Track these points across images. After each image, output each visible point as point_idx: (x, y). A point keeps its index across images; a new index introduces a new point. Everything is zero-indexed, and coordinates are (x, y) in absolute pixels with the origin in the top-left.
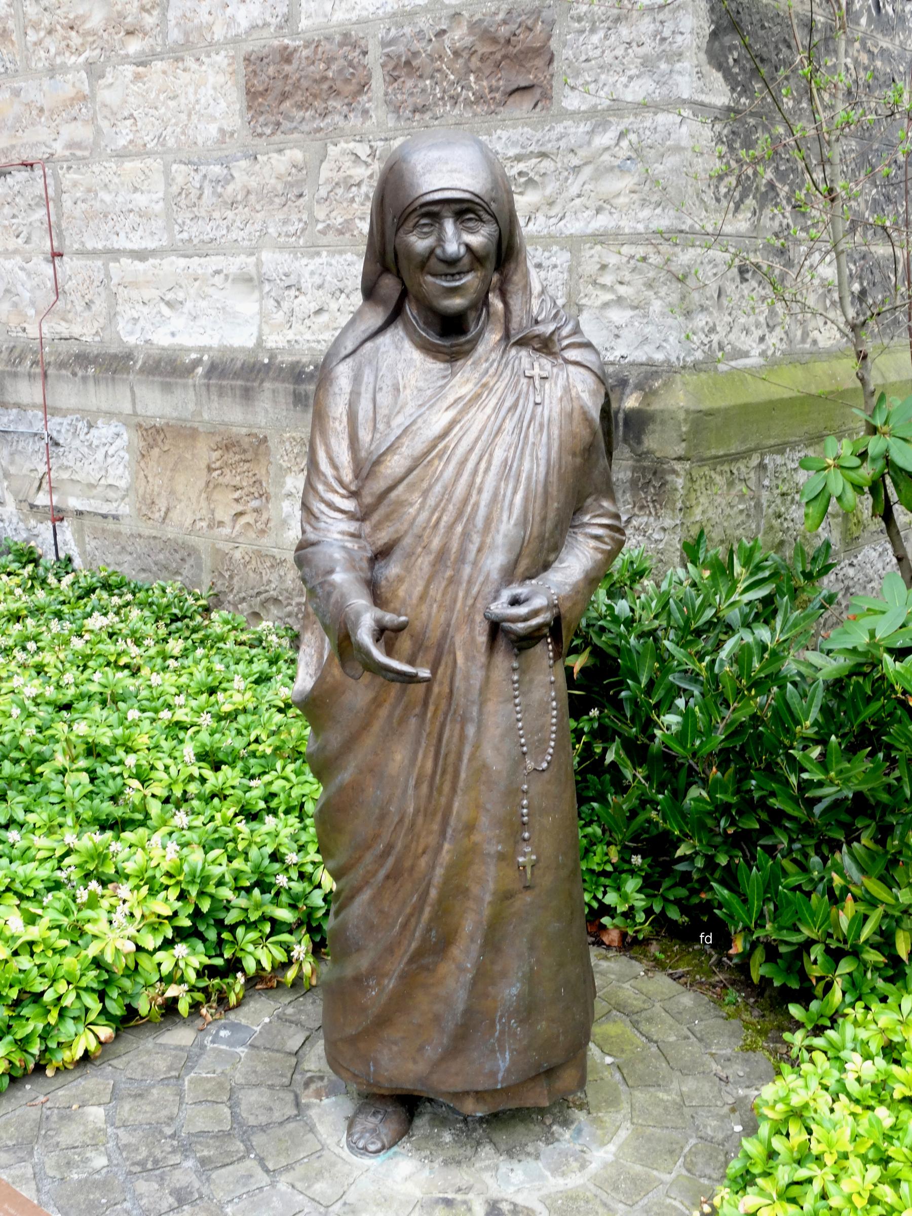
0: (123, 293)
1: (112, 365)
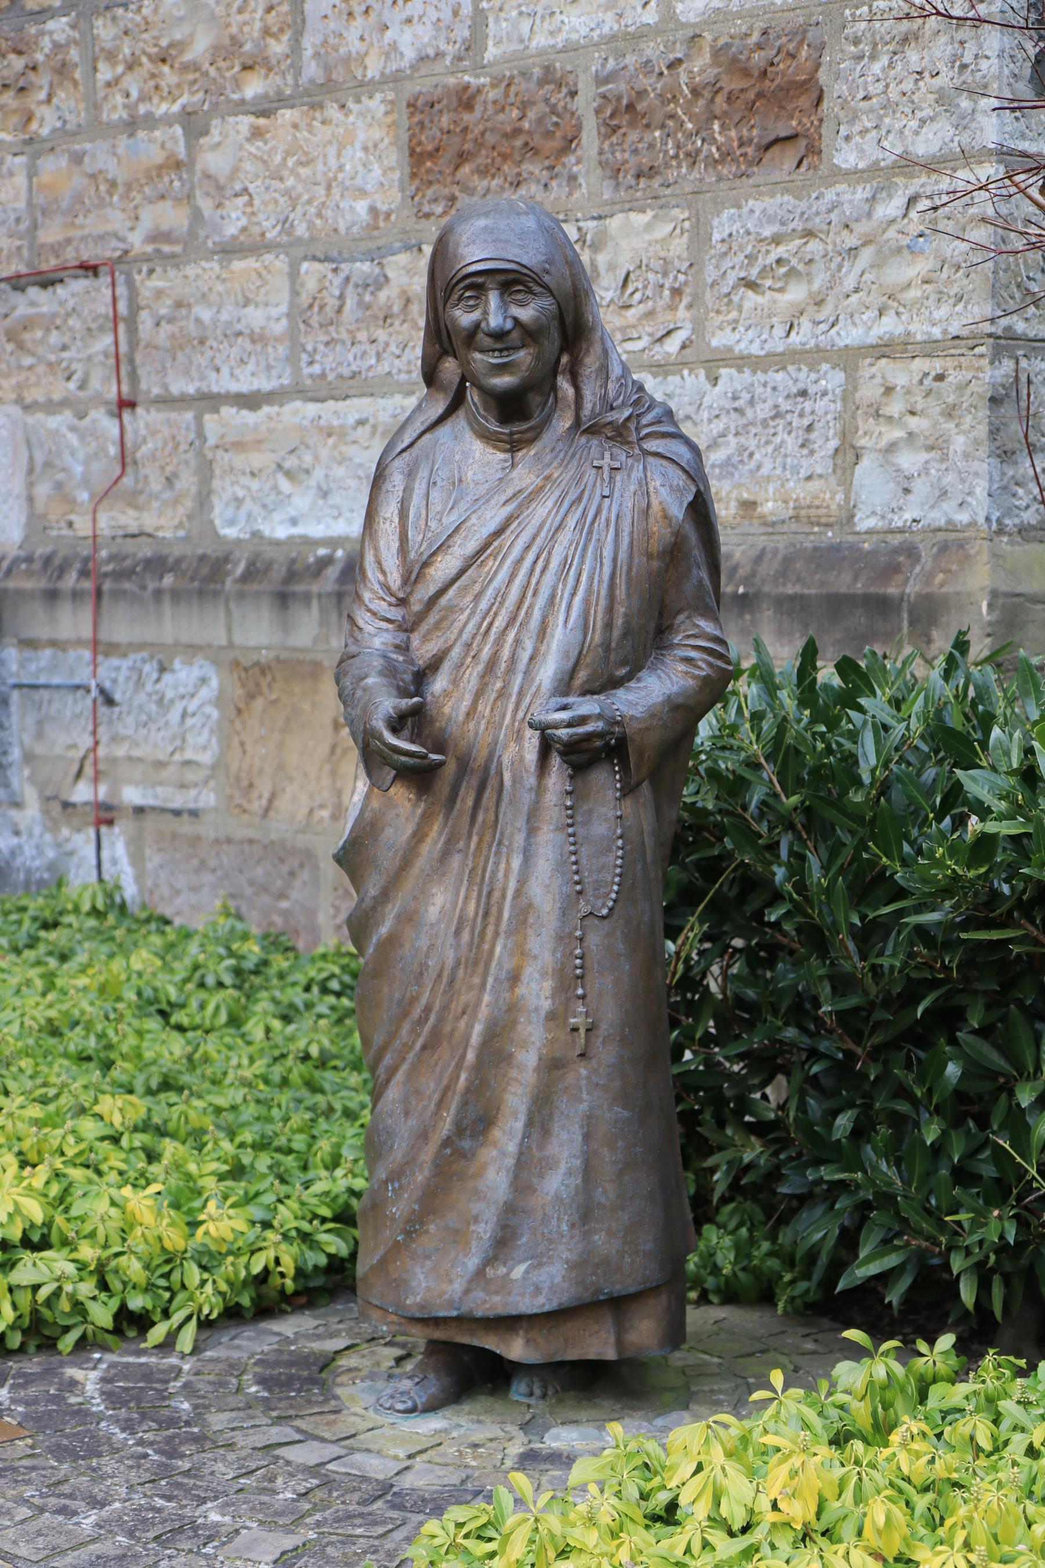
0: (223, 458)
1: (205, 576)
